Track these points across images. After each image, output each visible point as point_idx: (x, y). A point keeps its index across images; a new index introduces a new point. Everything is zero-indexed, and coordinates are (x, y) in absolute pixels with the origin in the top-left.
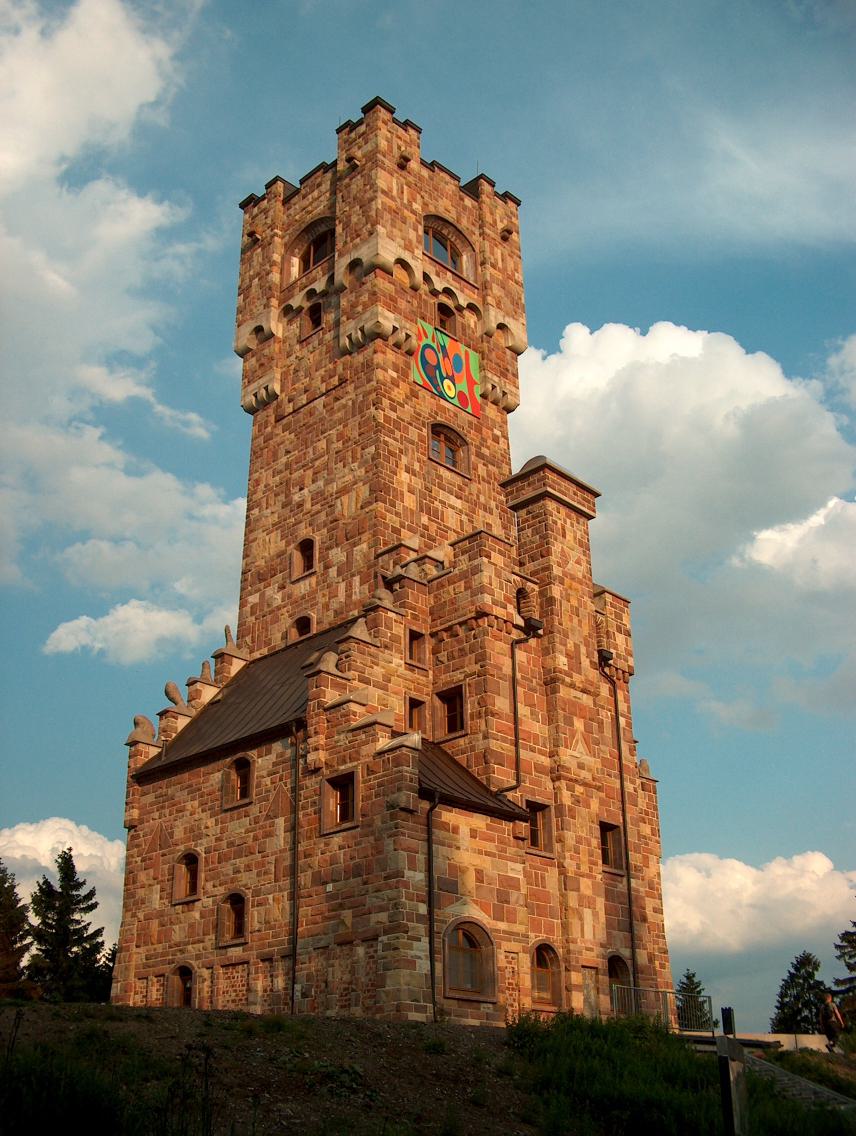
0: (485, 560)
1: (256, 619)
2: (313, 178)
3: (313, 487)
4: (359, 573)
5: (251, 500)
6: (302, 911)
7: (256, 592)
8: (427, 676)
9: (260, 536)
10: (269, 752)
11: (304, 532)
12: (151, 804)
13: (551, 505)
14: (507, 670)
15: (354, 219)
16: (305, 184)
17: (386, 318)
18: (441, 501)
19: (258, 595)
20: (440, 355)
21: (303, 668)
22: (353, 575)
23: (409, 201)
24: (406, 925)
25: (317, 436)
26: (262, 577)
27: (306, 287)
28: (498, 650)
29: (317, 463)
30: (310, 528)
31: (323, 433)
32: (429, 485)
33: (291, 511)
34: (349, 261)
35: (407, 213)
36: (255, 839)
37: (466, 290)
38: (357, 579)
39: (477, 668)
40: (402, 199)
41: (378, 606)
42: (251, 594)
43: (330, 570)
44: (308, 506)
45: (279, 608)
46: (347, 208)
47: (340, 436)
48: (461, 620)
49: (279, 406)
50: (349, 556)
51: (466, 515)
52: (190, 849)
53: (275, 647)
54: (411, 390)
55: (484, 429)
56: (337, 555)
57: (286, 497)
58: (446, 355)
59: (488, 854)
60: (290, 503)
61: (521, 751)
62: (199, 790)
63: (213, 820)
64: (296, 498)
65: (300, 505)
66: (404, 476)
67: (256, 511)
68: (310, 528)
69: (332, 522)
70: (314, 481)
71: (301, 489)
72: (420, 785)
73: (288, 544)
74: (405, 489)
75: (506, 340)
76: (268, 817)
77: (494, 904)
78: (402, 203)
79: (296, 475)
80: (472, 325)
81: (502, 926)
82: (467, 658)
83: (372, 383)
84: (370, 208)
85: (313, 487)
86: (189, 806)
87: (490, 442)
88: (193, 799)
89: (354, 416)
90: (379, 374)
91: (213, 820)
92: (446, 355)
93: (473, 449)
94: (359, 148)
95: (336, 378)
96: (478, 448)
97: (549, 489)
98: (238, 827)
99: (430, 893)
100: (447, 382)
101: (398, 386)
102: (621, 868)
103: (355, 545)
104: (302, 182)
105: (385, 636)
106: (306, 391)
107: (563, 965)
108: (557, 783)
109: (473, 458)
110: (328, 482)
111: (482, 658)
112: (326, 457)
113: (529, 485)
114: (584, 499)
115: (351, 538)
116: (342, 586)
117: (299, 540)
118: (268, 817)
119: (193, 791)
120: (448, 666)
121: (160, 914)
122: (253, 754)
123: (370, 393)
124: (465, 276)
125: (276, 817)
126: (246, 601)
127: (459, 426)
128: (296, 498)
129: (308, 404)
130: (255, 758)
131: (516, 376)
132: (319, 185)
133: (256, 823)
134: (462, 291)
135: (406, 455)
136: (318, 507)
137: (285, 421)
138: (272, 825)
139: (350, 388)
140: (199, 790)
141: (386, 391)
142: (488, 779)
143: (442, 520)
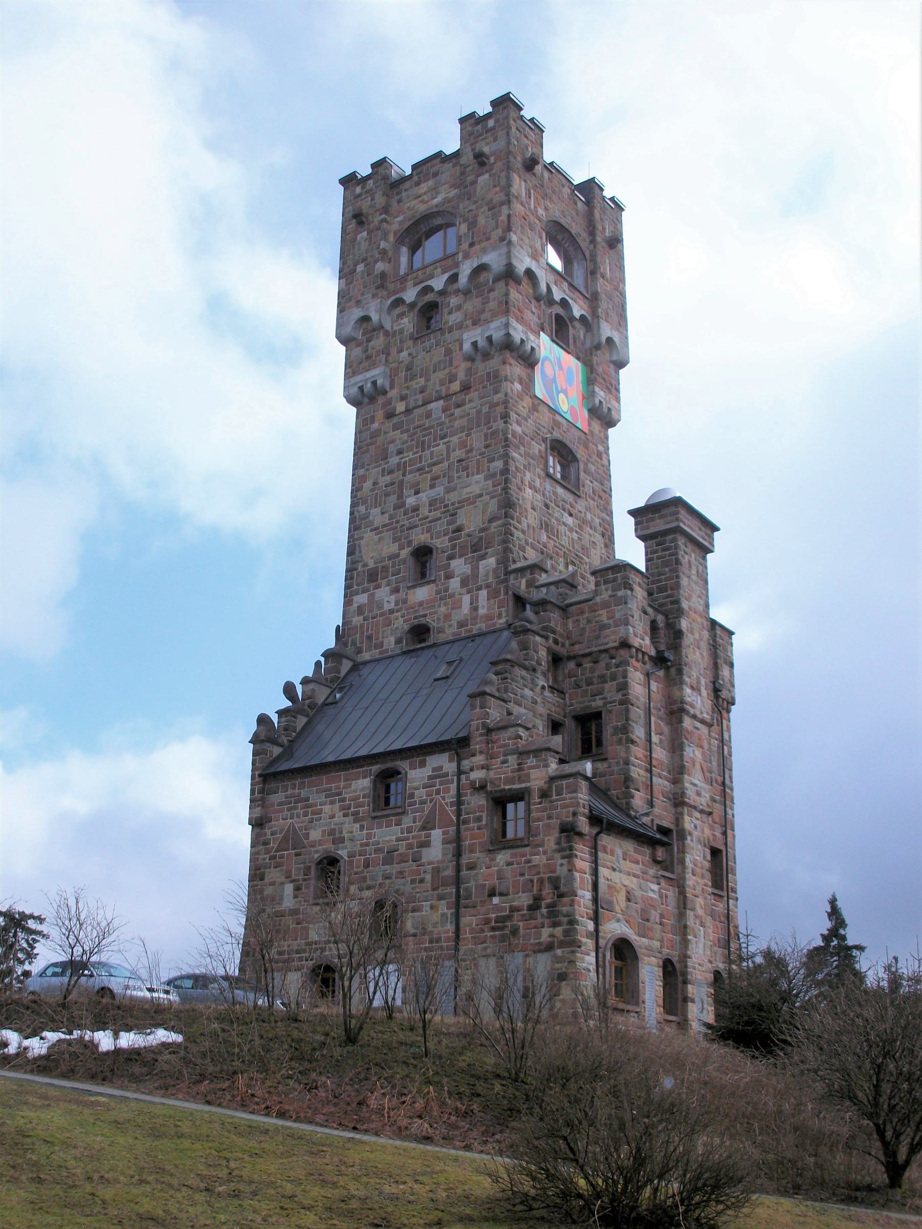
0: (629, 592)
1: (365, 619)
2: (429, 165)
3: (432, 493)
4: (488, 586)
5: (356, 496)
6: (465, 920)
7: (363, 592)
8: (564, 699)
9: (366, 535)
10: (423, 764)
11: (420, 537)
12: (280, 804)
13: (681, 541)
14: (643, 699)
15: (482, 221)
16: (418, 170)
17: (515, 329)
18: (557, 519)
19: (366, 595)
20: (556, 368)
21: (435, 680)
22: (479, 588)
23: (535, 207)
24: (580, 941)
25: (435, 440)
26: (373, 576)
27: (422, 282)
28: (636, 677)
29: (435, 469)
30: (428, 535)
31: (442, 438)
32: (548, 502)
33: (405, 514)
34: (475, 265)
35: (533, 219)
36: (410, 847)
37: (578, 300)
38: (483, 593)
39: (619, 696)
40: (529, 204)
41: (528, 630)
42: (357, 594)
43: (452, 580)
44: (424, 511)
45: (391, 612)
46: (473, 207)
47: (463, 445)
48: (602, 648)
49: (389, 402)
50: (475, 569)
51: (577, 532)
52: (330, 852)
53: (387, 651)
54: (533, 404)
55: (590, 444)
56: (459, 566)
57: (398, 499)
58: (561, 368)
59: (635, 876)
60: (403, 505)
61: (654, 779)
62: (339, 794)
63: (358, 825)
64: (411, 501)
65: (416, 509)
66: (529, 492)
67: (362, 509)
68: (428, 535)
69: (454, 532)
70: (432, 487)
71: (417, 493)
72: (591, 811)
73: (401, 548)
74: (529, 507)
75: (611, 353)
76: (424, 828)
77: (639, 923)
78: (529, 209)
79: (409, 478)
80: (582, 337)
81: (645, 941)
82: (606, 685)
83: (499, 395)
84: (500, 211)
85: (432, 493)
86: (327, 808)
87: (595, 457)
88: (332, 803)
89: (478, 426)
90: (506, 386)
91: (358, 825)
92: (561, 368)
93: (582, 466)
94: (488, 144)
95: (458, 382)
96: (586, 464)
97: (682, 525)
98: (387, 835)
99: (596, 912)
100: (561, 396)
101: (522, 400)
102: (722, 890)
103: (483, 557)
104: (414, 167)
105: (532, 659)
106: (422, 392)
107: (680, 979)
108: (679, 809)
109: (582, 474)
110: (448, 490)
111: (623, 687)
112: (446, 464)
113: (660, 517)
114: (706, 534)
115: (477, 548)
116: (466, 599)
117: (415, 544)
118: (424, 828)
119: (333, 795)
120: (587, 691)
121: (294, 912)
122: (403, 765)
123: (497, 404)
124: (575, 284)
125: (433, 828)
126: (352, 600)
127: (571, 441)
128: (411, 501)
129: (423, 405)
130: (407, 770)
131: (618, 390)
132: (436, 174)
133: (408, 832)
134: (576, 302)
135: (529, 471)
136: (437, 514)
137: (395, 420)
138: (429, 836)
139: (474, 395)
140: (339, 794)
141: (513, 405)
142: (628, 804)
143: (558, 538)
